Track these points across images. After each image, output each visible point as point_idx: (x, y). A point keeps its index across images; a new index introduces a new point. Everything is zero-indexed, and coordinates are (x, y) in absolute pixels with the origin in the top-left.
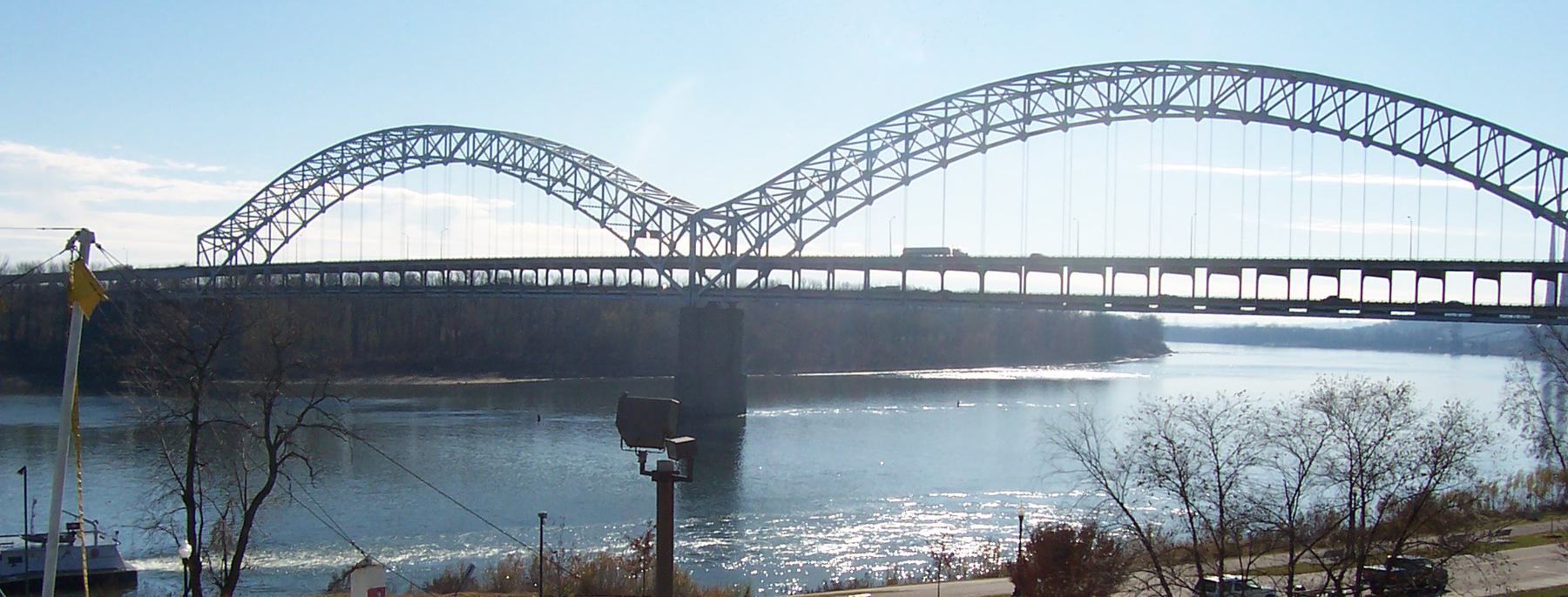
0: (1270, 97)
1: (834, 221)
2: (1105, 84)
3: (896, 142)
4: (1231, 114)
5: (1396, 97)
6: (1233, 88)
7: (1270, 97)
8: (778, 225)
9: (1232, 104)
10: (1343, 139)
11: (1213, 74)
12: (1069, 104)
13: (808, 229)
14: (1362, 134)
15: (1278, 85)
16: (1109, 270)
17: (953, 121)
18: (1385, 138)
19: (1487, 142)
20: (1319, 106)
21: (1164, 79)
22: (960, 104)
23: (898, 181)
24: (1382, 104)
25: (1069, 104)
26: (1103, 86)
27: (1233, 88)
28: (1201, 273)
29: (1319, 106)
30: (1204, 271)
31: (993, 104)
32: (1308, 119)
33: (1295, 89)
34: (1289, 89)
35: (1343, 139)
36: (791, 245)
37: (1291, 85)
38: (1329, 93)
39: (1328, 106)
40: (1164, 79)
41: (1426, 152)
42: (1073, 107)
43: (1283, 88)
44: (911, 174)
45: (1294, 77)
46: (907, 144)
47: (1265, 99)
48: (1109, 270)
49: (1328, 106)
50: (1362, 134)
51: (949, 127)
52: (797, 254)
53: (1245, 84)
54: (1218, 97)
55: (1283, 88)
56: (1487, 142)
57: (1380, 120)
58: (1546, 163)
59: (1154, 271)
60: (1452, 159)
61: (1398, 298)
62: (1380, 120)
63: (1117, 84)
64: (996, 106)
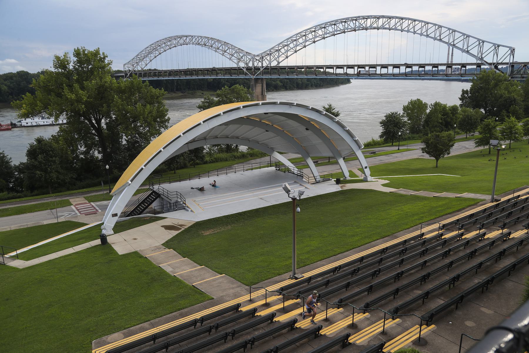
0: (385, 22)
1: (287, 57)
2: (355, 21)
3: (285, 47)
4: (375, 28)
5: (415, 21)
6: (375, 22)
7: (385, 22)
8: (273, 59)
9: (375, 25)
10: (402, 31)
11: (371, 18)
12: (325, 32)
13: (281, 59)
14: (420, 32)
15: (387, 20)
16: (335, 68)
17: (298, 40)
18: (399, 28)
19: (437, 29)
20: (397, 24)
21: (395, 20)
22: (300, 35)
23: (303, 47)
24: (412, 22)
25: (325, 32)
26: (333, 26)
27: (375, 22)
28: (356, 68)
29: (397, 24)
30: (357, 67)
31: (307, 34)
32: (406, 29)
33: (390, 21)
34: (389, 21)
35: (402, 31)
36: (277, 63)
37: (389, 20)
38: (399, 20)
39: (399, 24)
40: (395, 20)
41: (436, 37)
42: (337, 30)
43: (387, 21)
44: (306, 45)
45: (390, 18)
46: (296, 42)
47: (383, 23)
48: (335, 68)
49: (399, 24)
50: (420, 32)
51: (297, 42)
52: (278, 65)
53: (378, 21)
54: (372, 23)
55: (387, 21)
56: (437, 29)
57: (411, 26)
58: (451, 33)
59: (345, 68)
60: (441, 38)
61: (401, 72)
62: (411, 26)
63: (337, 26)
64: (328, 27)
